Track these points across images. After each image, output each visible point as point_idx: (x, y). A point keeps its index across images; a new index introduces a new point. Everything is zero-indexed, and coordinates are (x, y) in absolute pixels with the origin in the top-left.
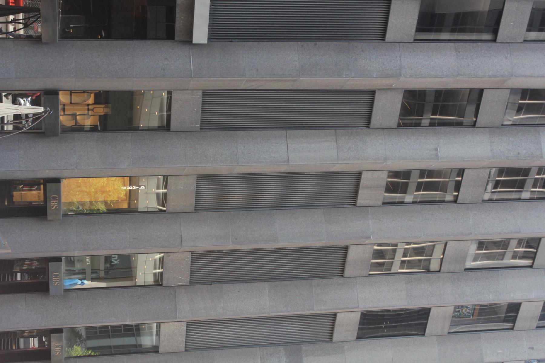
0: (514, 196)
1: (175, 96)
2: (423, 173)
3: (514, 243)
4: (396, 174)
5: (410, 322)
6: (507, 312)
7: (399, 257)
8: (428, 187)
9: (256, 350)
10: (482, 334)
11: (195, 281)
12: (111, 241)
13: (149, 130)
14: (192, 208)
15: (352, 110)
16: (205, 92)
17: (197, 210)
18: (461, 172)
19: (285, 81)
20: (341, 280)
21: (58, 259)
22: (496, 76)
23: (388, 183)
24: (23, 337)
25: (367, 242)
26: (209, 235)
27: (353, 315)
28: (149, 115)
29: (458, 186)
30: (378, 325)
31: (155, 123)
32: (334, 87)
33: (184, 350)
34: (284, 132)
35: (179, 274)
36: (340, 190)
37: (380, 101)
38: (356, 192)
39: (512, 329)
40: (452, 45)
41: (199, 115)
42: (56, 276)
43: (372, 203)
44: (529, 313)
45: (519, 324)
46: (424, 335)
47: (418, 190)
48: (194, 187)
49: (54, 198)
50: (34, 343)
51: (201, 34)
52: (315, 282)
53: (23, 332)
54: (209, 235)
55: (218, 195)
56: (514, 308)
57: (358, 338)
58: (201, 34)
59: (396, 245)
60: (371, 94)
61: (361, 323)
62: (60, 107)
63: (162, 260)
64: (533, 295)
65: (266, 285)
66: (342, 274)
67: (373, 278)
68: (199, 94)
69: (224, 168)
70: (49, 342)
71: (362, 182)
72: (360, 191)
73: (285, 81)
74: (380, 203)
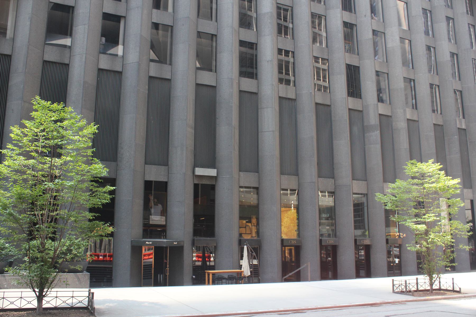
0: (291, 31)
1: (242, 185)
2: (280, 72)
3: (317, 65)
4: (280, 32)
5: (353, 73)
6: (348, 28)
7: (321, 83)
8: (287, 70)
9: (366, 147)
10: (359, 39)
11: (332, 176)
12: (312, 216)
13: (258, 199)
14: (296, 177)
15: (249, 102)
16: (240, 171)
17: (297, 175)
18: (280, 51)
19: (234, 132)
20: (332, 106)
21: (321, 241)
22: (233, 34)
23: (285, 84)
24: (359, 258)
25: (313, 94)
26: (309, 169)
27: (349, 101)
28: (252, 199)
29: (287, 53)
30: (354, 88)
31: (255, 196)
32: (238, 109)
33: (366, 182)
34: (260, 133)
35: (329, 184)
36: (288, 107)
37: (244, 88)
38: (289, 99)
39: (356, 25)
40: (218, 55)
41: (251, 173)
42: (329, 242)
43: (294, 91)
44: (347, 17)
45: (353, 22)
46: (359, 67)
47: (289, 75)
48: (286, 176)
49: (291, 242)
50: (363, 253)
51: (212, 172)
52: (333, 119)
53: (356, 257)
54: (309, 169)
55: (290, 164)
56: (346, 24)
57: (361, 98)
58: (212, 172)
59: (314, 66)
60: (241, 92)
61: (354, 97)
62: (252, 238)
63: (321, 192)
64: (339, 15)
65: (334, 142)
66: (329, 106)
67: (331, 91)
68: (242, 174)
69: (277, 162)
70: (361, 245)
71: (284, 96)
72: (289, 97)
73: (234, 132)
74: (294, 88)
